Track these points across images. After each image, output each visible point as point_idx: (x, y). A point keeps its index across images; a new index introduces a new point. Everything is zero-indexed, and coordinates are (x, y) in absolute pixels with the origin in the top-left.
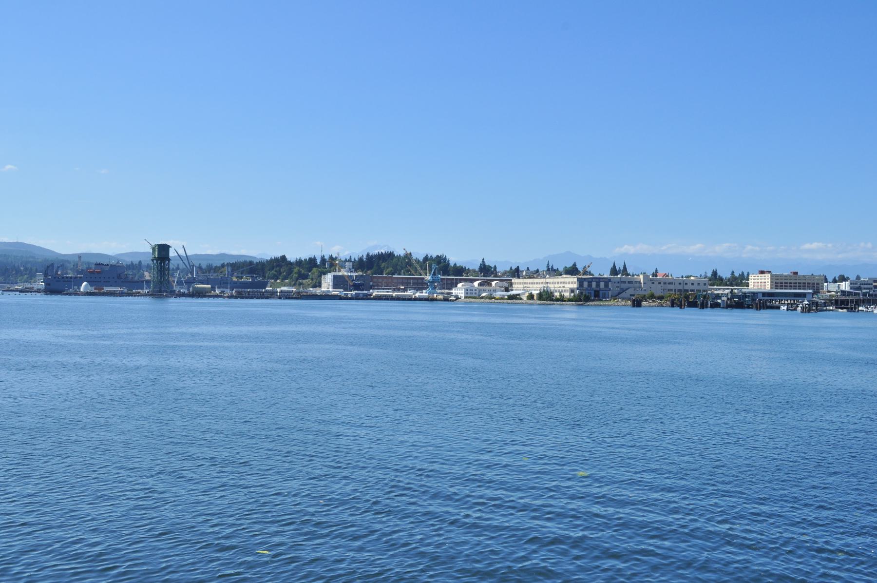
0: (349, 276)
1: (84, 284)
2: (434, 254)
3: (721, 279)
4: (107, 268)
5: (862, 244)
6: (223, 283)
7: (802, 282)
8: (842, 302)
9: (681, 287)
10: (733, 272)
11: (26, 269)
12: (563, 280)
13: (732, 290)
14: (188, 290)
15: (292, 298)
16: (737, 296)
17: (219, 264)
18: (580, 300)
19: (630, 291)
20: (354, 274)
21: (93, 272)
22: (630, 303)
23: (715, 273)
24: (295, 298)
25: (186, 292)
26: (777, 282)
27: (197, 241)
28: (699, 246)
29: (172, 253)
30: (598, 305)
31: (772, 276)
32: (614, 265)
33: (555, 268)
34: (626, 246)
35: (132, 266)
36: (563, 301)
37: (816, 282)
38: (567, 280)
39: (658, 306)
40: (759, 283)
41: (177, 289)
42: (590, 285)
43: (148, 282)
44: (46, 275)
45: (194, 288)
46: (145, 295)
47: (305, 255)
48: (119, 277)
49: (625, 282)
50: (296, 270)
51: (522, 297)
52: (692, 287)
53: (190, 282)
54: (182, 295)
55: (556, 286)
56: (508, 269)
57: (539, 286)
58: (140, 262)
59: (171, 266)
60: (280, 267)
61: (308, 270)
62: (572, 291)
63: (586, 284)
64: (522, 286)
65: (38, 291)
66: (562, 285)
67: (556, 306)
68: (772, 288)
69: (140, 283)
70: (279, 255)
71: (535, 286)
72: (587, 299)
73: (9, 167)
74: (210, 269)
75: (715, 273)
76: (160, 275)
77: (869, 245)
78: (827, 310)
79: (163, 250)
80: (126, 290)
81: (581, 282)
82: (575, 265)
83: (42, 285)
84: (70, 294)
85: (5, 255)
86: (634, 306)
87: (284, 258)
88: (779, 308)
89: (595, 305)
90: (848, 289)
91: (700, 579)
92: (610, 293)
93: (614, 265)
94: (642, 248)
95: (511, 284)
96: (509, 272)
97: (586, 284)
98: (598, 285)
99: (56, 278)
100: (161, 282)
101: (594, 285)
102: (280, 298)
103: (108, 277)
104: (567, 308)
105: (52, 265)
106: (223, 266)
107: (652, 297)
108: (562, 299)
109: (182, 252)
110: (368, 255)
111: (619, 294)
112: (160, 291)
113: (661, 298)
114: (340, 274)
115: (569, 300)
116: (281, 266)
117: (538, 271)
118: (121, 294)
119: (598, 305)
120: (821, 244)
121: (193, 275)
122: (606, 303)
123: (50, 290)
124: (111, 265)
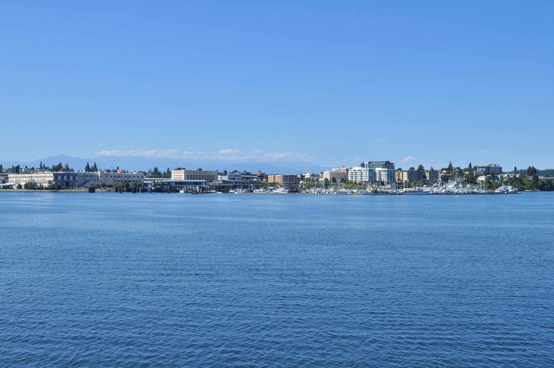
2: (524, 166)
3: (160, 174)
5: (256, 151)
7: (204, 175)
8: (223, 187)
9: (126, 179)
10: (168, 169)
12: (43, 175)
13: (155, 180)
16: (159, 185)
18: (54, 189)
19: (90, 183)
22: (88, 190)
23: (156, 169)
26: (189, 175)
28: (153, 151)
30: (67, 192)
31: (185, 171)
32: (88, 165)
33: (46, 166)
34: (104, 151)
36: (42, 189)
37: (212, 175)
38: (47, 175)
39: (107, 192)
40: (178, 176)
42: (62, 178)
49: (88, 176)
51: (13, 187)
52: (134, 179)
55: (39, 179)
56: (11, 167)
57: (27, 179)
62: (50, 182)
63: (59, 178)
64: (15, 179)
66: (43, 179)
67: (37, 193)
68: (185, 179)
71: (23, 179)
72: (59, 188)
75: (156, 169)
77: (260, 151)
78: (210, 193)
81: (56, 176)
82: (60, 164)
86: (90, 192)
87: (501, 168)
88: (179, 191)
89: (64, 192)
90: (227, 179)
91: (484, 366)
92: (77, 183)
93: (88, 165)
94: (106, 153)
95: (7, 178)
96: (11, 169)
97: (59, 178)
98: (68, 178)
101: (65, 178)
104: (46, 195)
107: (104, 186)
108: (41, 188)
111: (84, 184)
113: (110, 186)
115: (47, 189)
117: (33, 169)
119: (67, 192)
120: (231, 151)
122: (73, 190)
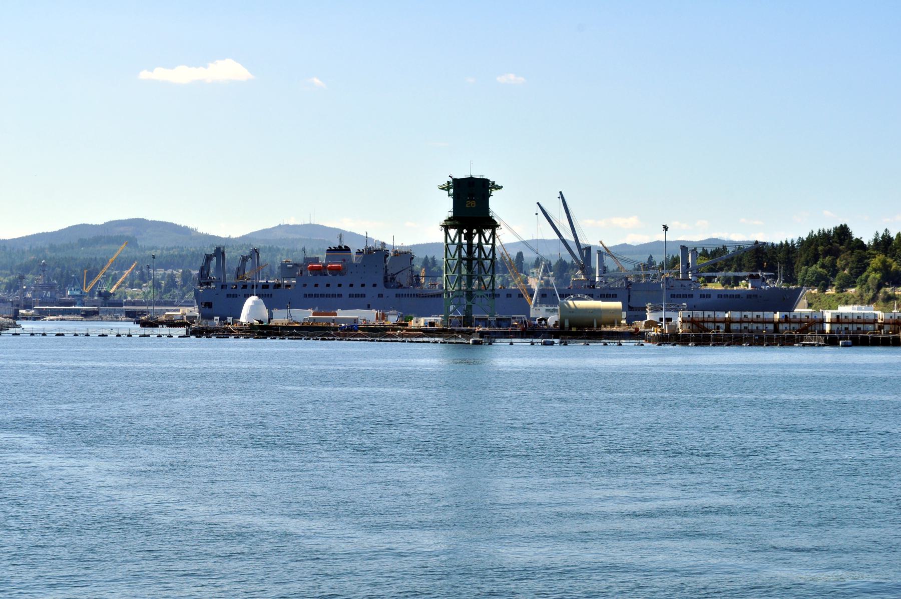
1: (251, 301)
21: (320, 271)
24: (885, 342)
45: (566, 311)
46: (429, 332)
50: (876, 262)
70: (829, 225)
87: (843, 232)
102: (832, 341)
105: (219, 253)
112: (468, 320)
116: (836, 254)
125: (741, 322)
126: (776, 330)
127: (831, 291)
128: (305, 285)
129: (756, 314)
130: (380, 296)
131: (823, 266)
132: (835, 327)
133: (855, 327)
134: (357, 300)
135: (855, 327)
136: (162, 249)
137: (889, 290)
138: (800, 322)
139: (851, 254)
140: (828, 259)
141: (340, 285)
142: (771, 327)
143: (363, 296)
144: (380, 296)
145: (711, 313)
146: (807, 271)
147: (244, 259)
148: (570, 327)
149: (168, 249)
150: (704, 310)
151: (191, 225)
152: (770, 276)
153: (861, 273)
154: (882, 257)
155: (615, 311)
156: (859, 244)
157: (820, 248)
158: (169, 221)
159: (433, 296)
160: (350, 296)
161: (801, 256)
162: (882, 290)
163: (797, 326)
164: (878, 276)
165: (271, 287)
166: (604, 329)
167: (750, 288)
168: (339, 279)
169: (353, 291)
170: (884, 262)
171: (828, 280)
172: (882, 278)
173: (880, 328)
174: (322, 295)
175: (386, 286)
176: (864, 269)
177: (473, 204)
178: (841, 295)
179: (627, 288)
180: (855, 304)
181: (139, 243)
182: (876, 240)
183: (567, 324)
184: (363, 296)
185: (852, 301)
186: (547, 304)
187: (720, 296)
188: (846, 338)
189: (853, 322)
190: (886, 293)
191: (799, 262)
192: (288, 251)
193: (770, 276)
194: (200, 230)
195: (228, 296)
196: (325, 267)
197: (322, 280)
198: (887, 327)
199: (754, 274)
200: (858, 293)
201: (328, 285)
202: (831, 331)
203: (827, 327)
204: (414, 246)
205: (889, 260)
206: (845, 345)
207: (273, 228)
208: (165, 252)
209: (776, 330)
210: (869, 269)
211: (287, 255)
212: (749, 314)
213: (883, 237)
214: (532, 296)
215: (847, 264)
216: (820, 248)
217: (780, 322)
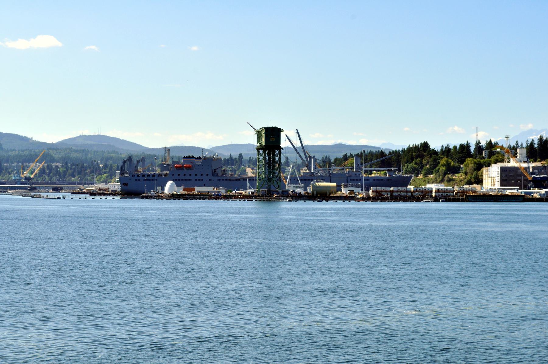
0: (527, 169)
1: (170, 183)
4: (199, 162)
6: (351, 180)
11: (106, 166)
14: (305, 189)
15: (454, 200)
17: (340, 155)
20: (532, 165)
21: (181, 168)
24: (458, 200)
25: (303, 192)
27: (319, 127)
29: (284, 143)
35: (231, 161)
41: (290, 188)
43: (252, 179)
44: (122, 173)
45: (314, 187)
46: (250, 198)
47: (455, 142)
48: (214, 173)
50: (443, 161)
53: (307, 179)
54: (297, 197)
58: (241, 156)
59: (283, 160)
60: (421, 156)
61: (466, 160)
65: (114, 193)
69: (242, 182)
70: (418, 141)
73: (93, 47)
74: (326, 162)
76: (269, 171)
79: (271, 137)
80: (223, 191)
83: (117, 187)
84: (150, 197)
85: (84, 151)
87: (425, 145)
99: (136, 177)
100: (269, 180)
102: (436, 200)
103: (200, 174)
105: (130, 159)
106: (345, 158)
109: (297, 144)
110: (541, 139)
112: (269, 192)
114: (509, 165)
116: (422, 157)
118: (218, 197)
121: (310, 169)
123: (128, 192)
124: (205, 158)
125: (397, 192)
126: (412, 195)
127: (420, 176)
128: (173, 175)
129: (403, 188)
130: (210, 180)
131: (416, 163)
132: (437, 194)
133: (445, 194)
134: (201, 182)
135: (445, 194)
136: (19, 151)
137: (450, 176)
138: (422, 192)
139: (430, 157)
140: (418, 160)
141: (190, 175)
142: (410, 194)
143: (202, 180)
144: (210, 180)
145: (384, 188)
146: (408, 166)
147: (125, 162)
148: (317, 194)
149: (22, 151)
150: (381, 187)
151: (29, 136)
152: (397, 170)
153: (435, 167)
154: (446, 159)
155: (333, 187)
156: (434, 152)
157: (414, 154)
158: (16, 133)
159: (236, 180)
160: (196, 180)
161: (404, 158)
162: (446, 176)
163: (421, 194)
164: (444, 168)
165: (151, 176)
166: (332, 195)
167: (388, 175)
168: (190, 172)
169: (197, 177)
170: (447, 162)
171: (419, 171)
172: (446, 169)
173: (456, 194)
174: (182, 180)
175: (213, 175)
176: (437, 165)
177: (274, 139)
178: (425, 178)
179: (330, 176)
180: (433, 183)
181: (4, 146)
182: (442, 150)
183: (315, 193)
184: (202, 180)
185: (431, 182)
186: (294, 184)
187: (374, 180)
188: (442, 199)
189: (444, 192)
190: (448, 177)
191: (403, 160)
192: (94, 152)
193: (397, 170)
194: (34, 139)
195: (136, 180)
196: (183, 166)
197: (181, 172)
198: (459, 194)
199: (390, 169)
200: (434, 178)
201: (185, 175)
202: (435, 196)
203: (434, 194)
204: (171, 147)
205: (450, 160)
206: (442, 201)
207: (77, 137)
208: (21, 153)
209: (412, 195)
210: (440, 165)
211: (94, 154)
212: (400, 188)
213: (446, 148)
214: (286, 180)
215: (428, 162)
216: (414, 154)
217: (414, 192)
